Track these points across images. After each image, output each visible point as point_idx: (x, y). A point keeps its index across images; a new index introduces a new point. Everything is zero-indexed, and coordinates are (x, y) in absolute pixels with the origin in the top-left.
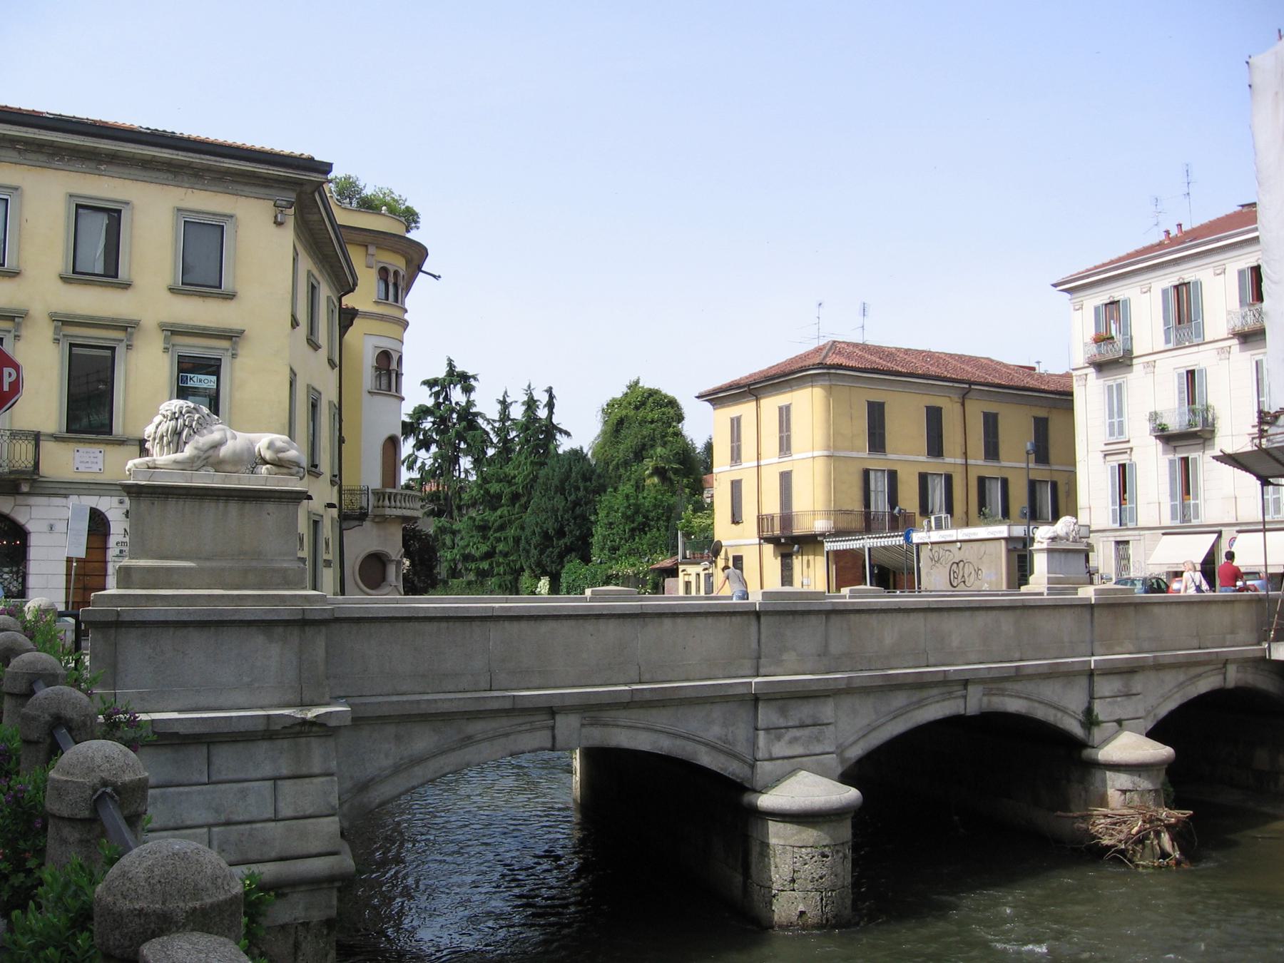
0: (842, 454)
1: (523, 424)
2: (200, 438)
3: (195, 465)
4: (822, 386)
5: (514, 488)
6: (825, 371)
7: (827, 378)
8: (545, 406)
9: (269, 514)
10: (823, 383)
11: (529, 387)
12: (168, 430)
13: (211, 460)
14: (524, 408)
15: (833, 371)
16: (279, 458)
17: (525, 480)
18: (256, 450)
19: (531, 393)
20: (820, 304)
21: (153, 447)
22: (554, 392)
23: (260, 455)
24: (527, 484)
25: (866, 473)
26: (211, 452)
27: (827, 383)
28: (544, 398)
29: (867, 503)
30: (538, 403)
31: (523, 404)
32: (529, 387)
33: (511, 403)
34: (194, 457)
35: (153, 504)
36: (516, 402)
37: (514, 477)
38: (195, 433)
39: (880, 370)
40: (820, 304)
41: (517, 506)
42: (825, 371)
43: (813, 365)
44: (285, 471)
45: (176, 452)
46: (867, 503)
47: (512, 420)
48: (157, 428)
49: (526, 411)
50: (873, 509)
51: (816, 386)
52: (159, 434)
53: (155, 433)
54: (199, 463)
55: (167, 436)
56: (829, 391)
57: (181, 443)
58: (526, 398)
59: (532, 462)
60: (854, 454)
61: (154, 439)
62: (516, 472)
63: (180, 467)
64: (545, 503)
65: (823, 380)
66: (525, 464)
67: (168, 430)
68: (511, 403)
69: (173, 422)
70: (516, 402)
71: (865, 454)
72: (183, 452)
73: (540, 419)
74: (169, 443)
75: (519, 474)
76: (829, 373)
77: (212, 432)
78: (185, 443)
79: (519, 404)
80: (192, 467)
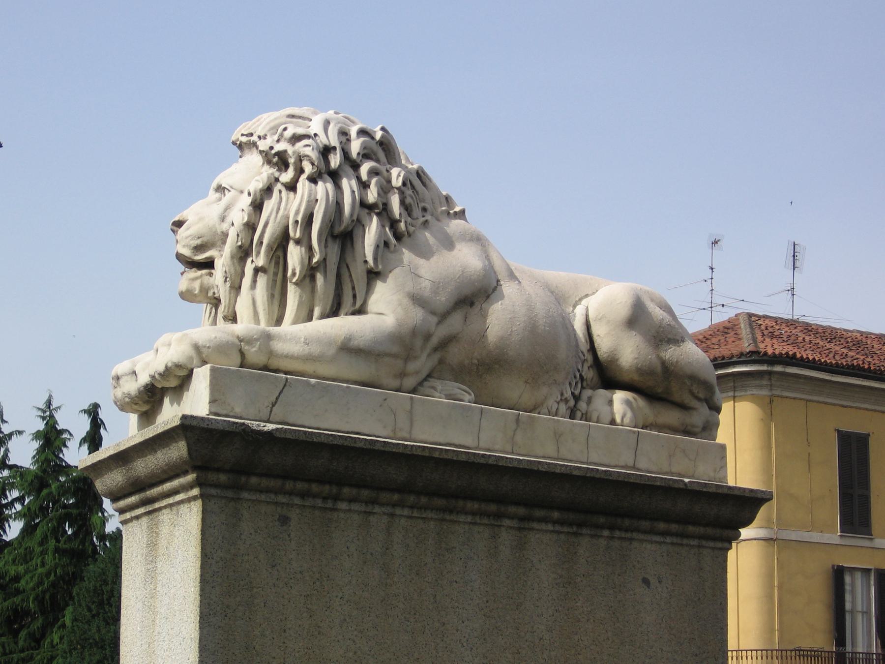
0: (793, 536)
1: (36, 476)
2: (421, 262)
3: (412, 367)
4: (754, 399)
5: (17, 600)
6: (764, 368)
7: (765, 382)
8: (83, 441)
9: (646, 582)
10: (755, 392)
11: (49, 403)
12: (309, 219)
13: (456, 354)
14: (36, 445)
15: (778, 368)
16: (663, 363)
17: (40, 583)
18: (578, 326)
19: (52, 416)
20: (715, 242)
21: (236, 288)
22: (102, 415)
23: (593, 349)
24: (44, 592)
25: (838, 574)
26: (455, 322)
27: (765, 392)
28: (80, 427)
29: (840, 638)
30: (65, 436)
31: (37, 435)
32: (49, 403)
33: (10, 435)
34: (414, 332)
35: (284, 520)
36: (20, 433)
37: (17, 579)
38: (398, 237)
39: (863, 369)
40: (715, 242)
41: (23, 634)
42: (764, 368)
43: (742, 354)
44: (672, 416)
45: (334, 311)
46: (840, 638)
47: (11, 467)
48: (257, 206)
49: (41, 451)
50: (849, 648)
51: (743, 398)
52: (268, 233)
53: (251, 227)
54: (422, 363)
55: (305, 241)
56: (769, 408)
57: (358, 273)
58: (41, 426)
59: (57, 550)
60: (815, 537)
61: (244, 253)
62: (21, 569)
63: (364, 375)
64: (99, 631)
65: (761, 387)
66: (43, 553)
67: (309, 219)
68: (10, 435)
69: (323, 189)
70: (20, 433)
71: (834, 537)
72: (360, 311)
73: (68, 466)
74: (310, 273)
75: (27, 571)
76: (770, 373)
77: (449, 243)
78: (373, 275)
79: (27, 437)
80: (402, 375)
